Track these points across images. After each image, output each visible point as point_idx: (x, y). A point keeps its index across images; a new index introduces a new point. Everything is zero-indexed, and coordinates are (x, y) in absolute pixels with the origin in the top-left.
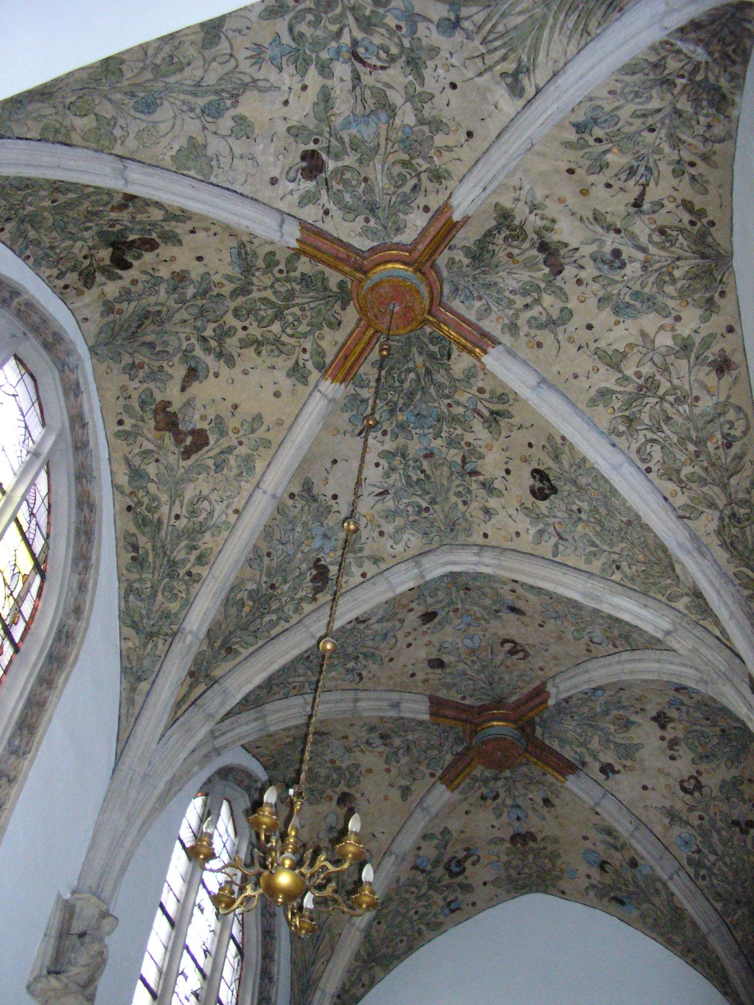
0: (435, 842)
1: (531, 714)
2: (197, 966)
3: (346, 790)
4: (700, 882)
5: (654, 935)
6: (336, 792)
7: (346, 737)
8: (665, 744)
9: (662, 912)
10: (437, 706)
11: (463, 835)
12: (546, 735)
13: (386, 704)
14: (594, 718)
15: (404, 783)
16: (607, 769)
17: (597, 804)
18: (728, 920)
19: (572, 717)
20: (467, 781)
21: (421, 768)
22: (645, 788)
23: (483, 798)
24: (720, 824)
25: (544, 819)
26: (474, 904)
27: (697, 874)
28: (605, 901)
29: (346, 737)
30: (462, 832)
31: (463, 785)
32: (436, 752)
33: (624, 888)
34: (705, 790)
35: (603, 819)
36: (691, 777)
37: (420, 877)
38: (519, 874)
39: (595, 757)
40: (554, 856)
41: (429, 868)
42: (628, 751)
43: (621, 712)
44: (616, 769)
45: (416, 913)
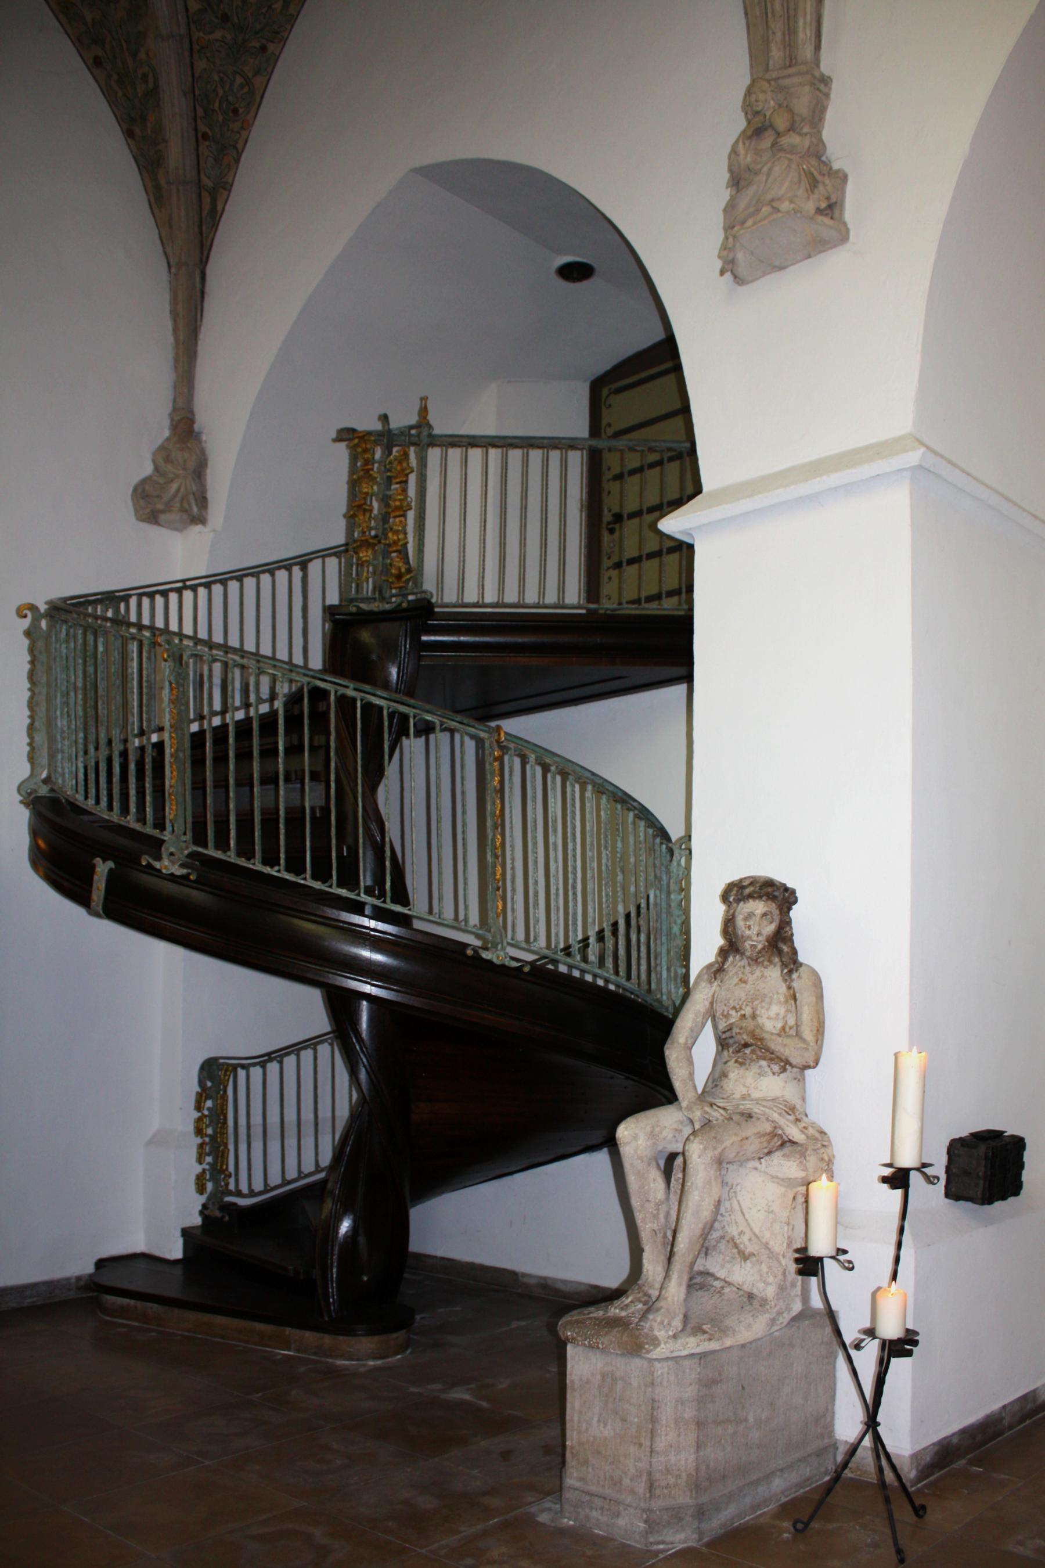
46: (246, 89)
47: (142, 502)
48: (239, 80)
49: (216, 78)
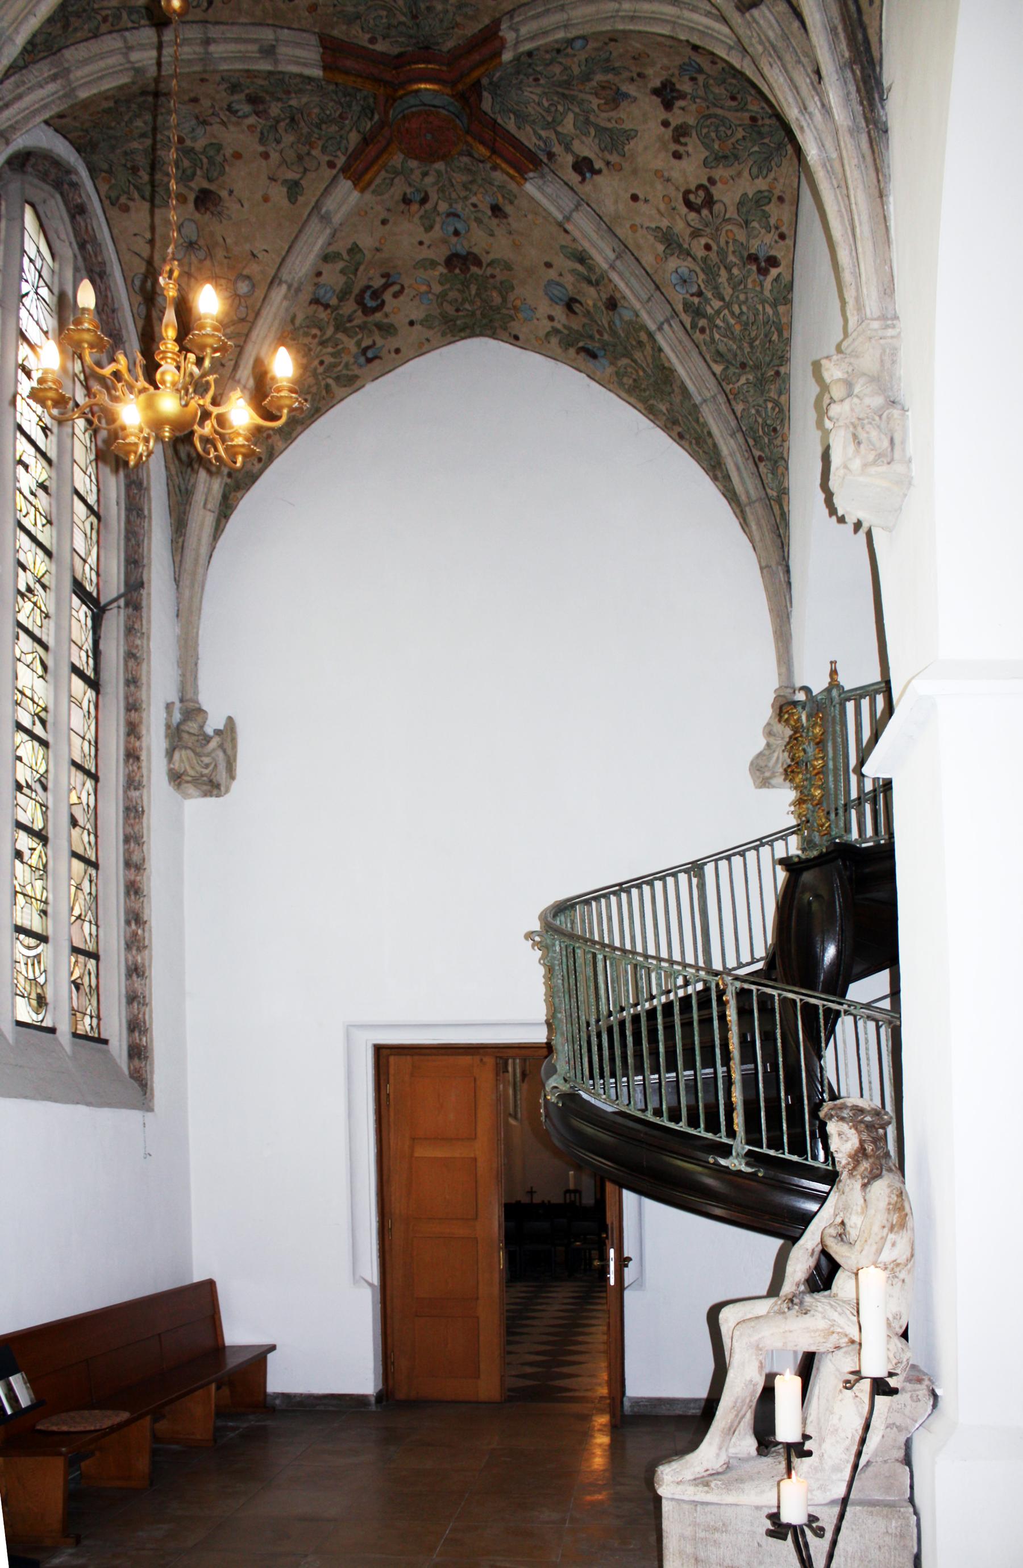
0: (340, 265)
1: (475, 74)
2: (38, 449)
3: (205, 185)
4: (697, 336)
5: (632, 400)
6: (191, 189)
7: (195, 100)
8: (668, 133)
9: (644, 371)
10: (334, 51)
11: (378, 255)
12: (497, 108)
13: (254, 47)
14: (568, 84)
15: (291, 175)
16: (583, 167)
17: (568, 219)
18: (728, 388)
19: (536, 80)
20: (383, 174)
21: (314, 152)
22: (635, 198)
23: (406, 201)
24: (731, 258)
25: (492, 235)
26: (397, 351)
27: (694, 326)
28: (572, 351)
29: (195, 100)
30: (378, 250)
31: (378, 181)
32: (334, 128)
33: (597, 337)
34: (716, 208)
35: (574, 240)
36: (700, 187)
37: (323, 315)
38: (457, 310)
39: (568, 149)
40: (505, 289)
41: (334, 302)
42: (615, 140)
43: (610, 77)
44: (597, 166)
45: (322, 363)
46: (777, 410)
47: (758, 773)
48: (770, 405)
49: (753, 411)
